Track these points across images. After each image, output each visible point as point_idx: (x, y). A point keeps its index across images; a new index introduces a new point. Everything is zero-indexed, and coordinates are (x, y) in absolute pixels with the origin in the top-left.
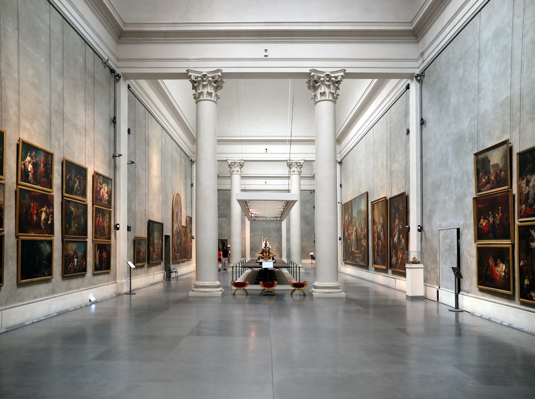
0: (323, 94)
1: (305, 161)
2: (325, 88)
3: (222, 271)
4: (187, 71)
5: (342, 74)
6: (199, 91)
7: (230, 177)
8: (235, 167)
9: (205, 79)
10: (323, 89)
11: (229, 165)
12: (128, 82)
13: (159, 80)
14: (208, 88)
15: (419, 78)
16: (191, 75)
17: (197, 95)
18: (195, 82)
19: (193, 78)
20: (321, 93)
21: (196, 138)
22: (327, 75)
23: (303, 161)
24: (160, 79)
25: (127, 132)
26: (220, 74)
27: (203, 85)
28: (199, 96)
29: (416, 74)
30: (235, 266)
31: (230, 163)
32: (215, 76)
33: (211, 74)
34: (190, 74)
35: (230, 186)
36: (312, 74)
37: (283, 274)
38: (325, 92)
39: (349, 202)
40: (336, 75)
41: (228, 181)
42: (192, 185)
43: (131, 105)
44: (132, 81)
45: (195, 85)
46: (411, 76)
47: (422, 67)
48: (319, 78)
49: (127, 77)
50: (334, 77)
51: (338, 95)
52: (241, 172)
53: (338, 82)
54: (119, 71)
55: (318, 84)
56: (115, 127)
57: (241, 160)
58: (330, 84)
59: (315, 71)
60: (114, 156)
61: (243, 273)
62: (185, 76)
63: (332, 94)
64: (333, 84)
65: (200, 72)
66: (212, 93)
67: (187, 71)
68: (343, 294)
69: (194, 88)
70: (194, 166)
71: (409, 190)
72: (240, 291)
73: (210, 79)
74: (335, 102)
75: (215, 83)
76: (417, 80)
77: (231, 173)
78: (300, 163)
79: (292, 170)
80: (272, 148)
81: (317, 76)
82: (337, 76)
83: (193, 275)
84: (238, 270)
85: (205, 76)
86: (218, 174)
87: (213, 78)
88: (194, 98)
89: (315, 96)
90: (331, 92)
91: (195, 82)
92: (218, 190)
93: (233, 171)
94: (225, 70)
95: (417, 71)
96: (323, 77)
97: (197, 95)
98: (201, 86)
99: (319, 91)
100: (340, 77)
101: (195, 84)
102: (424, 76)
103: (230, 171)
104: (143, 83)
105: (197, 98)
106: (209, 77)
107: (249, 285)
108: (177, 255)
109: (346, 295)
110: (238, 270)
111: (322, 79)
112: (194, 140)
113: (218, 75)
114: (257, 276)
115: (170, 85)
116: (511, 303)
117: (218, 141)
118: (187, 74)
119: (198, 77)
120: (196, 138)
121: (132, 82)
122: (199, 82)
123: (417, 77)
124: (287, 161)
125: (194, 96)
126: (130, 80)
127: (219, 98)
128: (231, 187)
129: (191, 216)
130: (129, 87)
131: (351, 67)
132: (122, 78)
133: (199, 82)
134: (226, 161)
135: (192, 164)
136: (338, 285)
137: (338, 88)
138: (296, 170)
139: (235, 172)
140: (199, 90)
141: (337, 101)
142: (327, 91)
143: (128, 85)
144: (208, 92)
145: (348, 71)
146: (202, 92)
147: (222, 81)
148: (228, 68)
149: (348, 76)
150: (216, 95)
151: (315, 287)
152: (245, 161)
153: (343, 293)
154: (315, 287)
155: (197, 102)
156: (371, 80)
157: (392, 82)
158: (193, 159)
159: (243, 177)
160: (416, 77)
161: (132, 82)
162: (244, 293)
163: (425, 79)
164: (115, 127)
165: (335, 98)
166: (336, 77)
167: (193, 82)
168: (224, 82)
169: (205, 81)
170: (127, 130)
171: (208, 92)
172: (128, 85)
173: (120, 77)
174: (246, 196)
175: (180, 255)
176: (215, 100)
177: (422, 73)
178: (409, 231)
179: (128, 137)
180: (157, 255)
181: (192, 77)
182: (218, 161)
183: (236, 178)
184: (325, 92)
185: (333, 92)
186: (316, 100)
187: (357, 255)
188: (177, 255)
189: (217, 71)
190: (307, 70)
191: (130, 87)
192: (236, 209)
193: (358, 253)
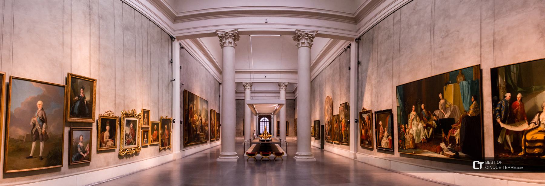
0: (303, 43)
1: (289, 83)
2: (304, 40)
3: (238, 144)
4: (216, 31)
5: (316, 33)
6: (223, 42)
7: (244, 93)
8: (247, 86)
9: (227, 35)
10: (303, 40)
11: (244, 85)
12: (179, 42)
13: (197, 39)
14: (229, 40)
15: (357, 41)
16: (218, 33)
17: (222, 44)
18: (221, 37)
19: (219, 35)
20: (302, 42)
21: (221, 70)
22: (306, 33)
23: (288, 83)
24: (198, 38)
25: (179, 68)
26: (237, 32)
27: (226, 38)
28: (224, 44)
29: (355, 39)
30: (248, 141)
31: (244, 84)
32: (234, 33)
33: (231, 32)
34: (217, 32)
35: (244, 97)
36: (297, 32)
37: (276, 146)
38: (304, 42)
39: (401, 86)
40: (312, 33)
41: (243, 95)
42: (220, 96)
43: (181, 56)
44: (182, 41)
45: (221, 38)
46: (351, 39)
47: (359, 35)
48: (281, 84)
49: (179, 38)
50: (310, 35)
51: (312, 44)
52: (251, 89)
53: (313, 38)
54: (174, 36)
55: (300, 38)
56: (172, 65)
57: (251, 82)
58: (308, 38)
59: (298, 30)
60: (172, 81)
61: (250, 146)
62: (215, 34)
63: (309, 44)
64: (309, 38)
65: (224, 32)
66: (232, 42)
67: (216, 31)
68: (315, 159)
69: (221, 40)
70: (221, 86)
71: (349, 101)
72: (252, 158)
73: (231, 35)
74: (311, 48)
75: (234, 37)
76: (356, 42)
77: (245, 89)
78: (286, 84)
79: (281, 88)
80: (269, 76)
81: (300, 33)
82: (312, 34)
83: (220, 147)
84: (248, 144)
85: (227, 33)
86: (236, 91)
87: (232, 34)
88: (221, 46)
89: (298, 44)
90: (308, 42)
91: (221, 37)
92: (236, 100)
93: (246, 88)
94: (239, 30)
95: (357, 37)
96: (304, 34)
97: (222, 44)
98: (225, 39)
99: (301, 41)
100: (314, 35)
101: (221, 38)
102: (360, 40)
103: (244, 89)
104: (188, 41)
105: (222, 46)
106: (229, 34)
107: (258, 154)
108: (328, 137)
109: (316, 160)
110: (248, 144)
111: (303, 35)
112: (221, 72)
113: (236, 32)
114: (260, 148)
115: (204, 41)
116: (488, 174)
117: (236, 72)
118: (215, 33)
119: (223, 34)
120: (222, 69)
121: (182, 41)
122: (224, 37)
123: (356, 40)
124: (278, 83)
125: (220, 45)
126: (181, 40)
127: (237, 45)
128: (245, 98)
129: (219, 113)
130: (180, 44)
131: (321, 31)
132: (176, 39)
133: (224, 37)
134: (242, 83)
135: (220, 85)
136: (311, 154)
137: (312, 41)
138: (283, 88)
139: (226, 44)
140: (224, 41)
141: (312, 47)
142: (306, 42)
143: (180, 43)
144: (229, 42)
145: (319, 32)
146: (225, 42)
147: (238, 36)
148: (241, 28)
149: (319, 35)
150: (235, 43)
151: (297, 155)
152: (253, 83)
153: (314, 159)
154: (297, 155)
155: (222, 48)
156: (330, 39)
157: (342, 42)
158: (220, 82)
159: (252, 92)
160: (356, 40)
161: (182, 41)
162: (253, 159)
163: (361, 42)
164: (172, 65)
165: (310, 46)
166: (312, 35)
167: (220, 37)
168: (240, 37)
169: (227, 36)
170: (179, 67)
171: (229, 42)
172: (180, 43)
173: (175, 38)
174: (252, 102)
175: (330, 137)
176: (234, 46)
177: (359, 38)
178: (350, 123)
179: (180, 71)
180: (317, 135)
181: (219, 34)
182: (236, 83)
183: (248, 92)
184: (304, 42)
185: (310, 42)
186: (299, 46)
187: (201, 136)
188: (328, 137)
189: (235, 30)
190: (294, 30)
191: (181, 44)
192: (248, 110)
193: (202, 135)
